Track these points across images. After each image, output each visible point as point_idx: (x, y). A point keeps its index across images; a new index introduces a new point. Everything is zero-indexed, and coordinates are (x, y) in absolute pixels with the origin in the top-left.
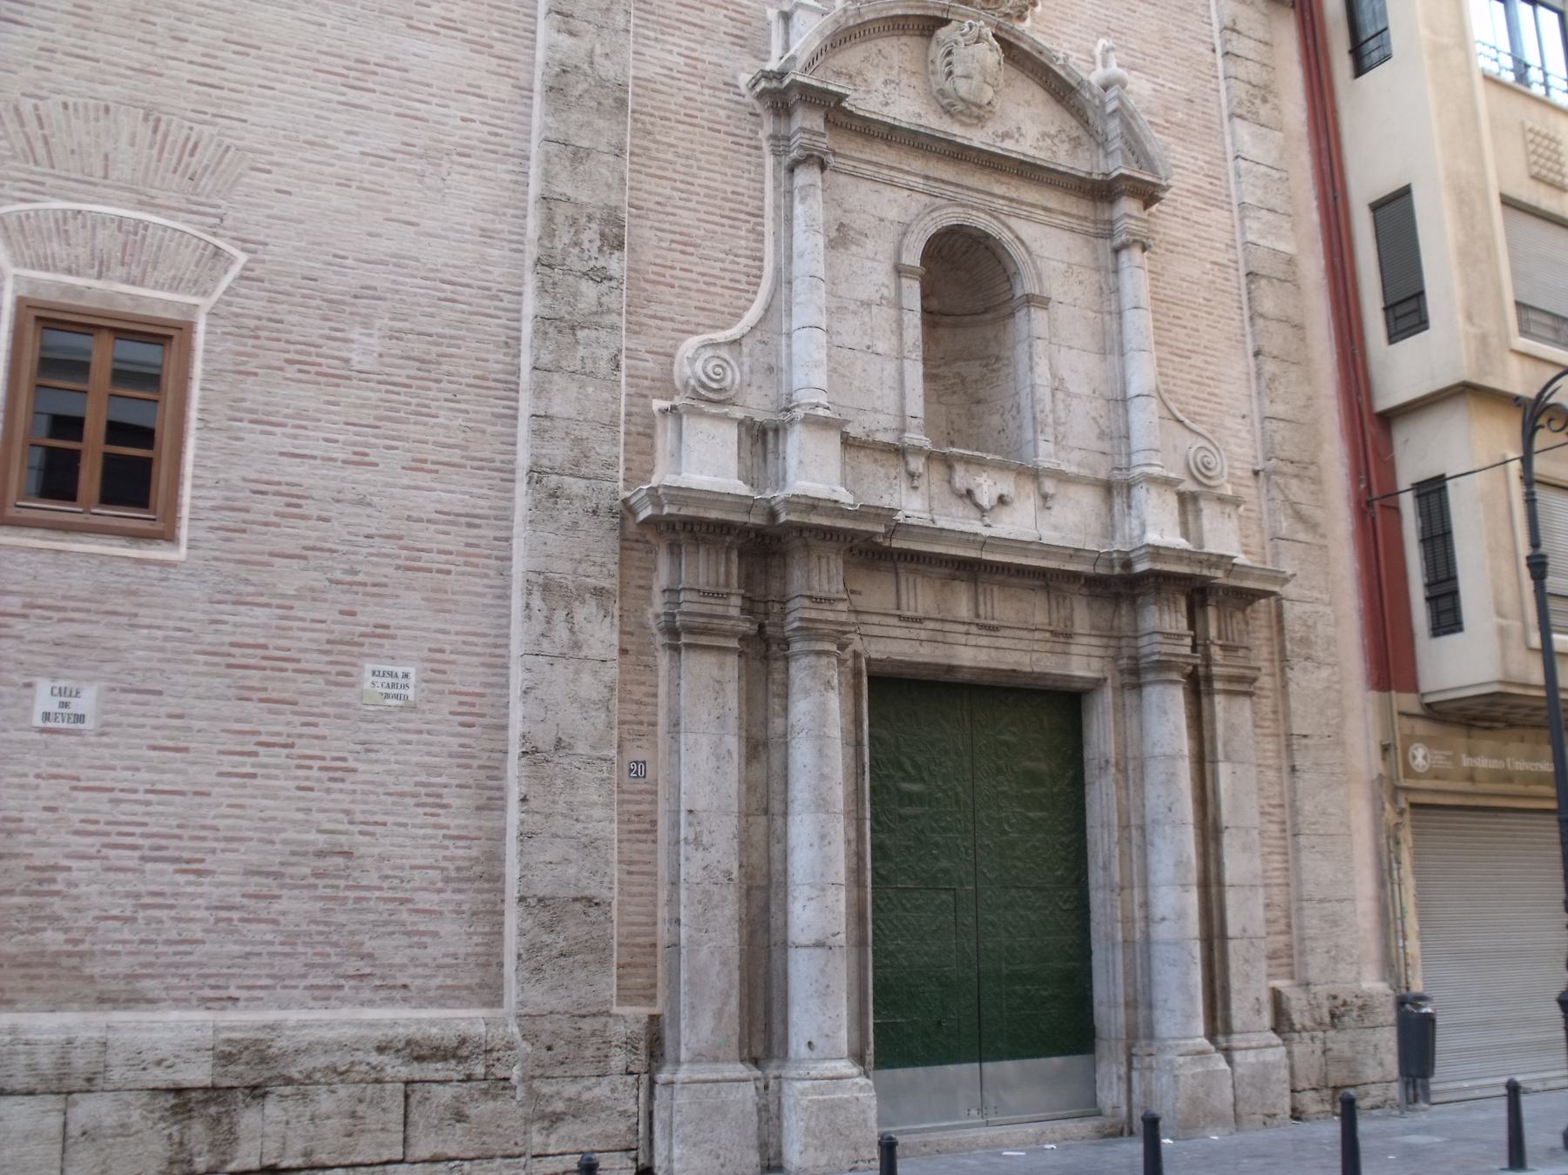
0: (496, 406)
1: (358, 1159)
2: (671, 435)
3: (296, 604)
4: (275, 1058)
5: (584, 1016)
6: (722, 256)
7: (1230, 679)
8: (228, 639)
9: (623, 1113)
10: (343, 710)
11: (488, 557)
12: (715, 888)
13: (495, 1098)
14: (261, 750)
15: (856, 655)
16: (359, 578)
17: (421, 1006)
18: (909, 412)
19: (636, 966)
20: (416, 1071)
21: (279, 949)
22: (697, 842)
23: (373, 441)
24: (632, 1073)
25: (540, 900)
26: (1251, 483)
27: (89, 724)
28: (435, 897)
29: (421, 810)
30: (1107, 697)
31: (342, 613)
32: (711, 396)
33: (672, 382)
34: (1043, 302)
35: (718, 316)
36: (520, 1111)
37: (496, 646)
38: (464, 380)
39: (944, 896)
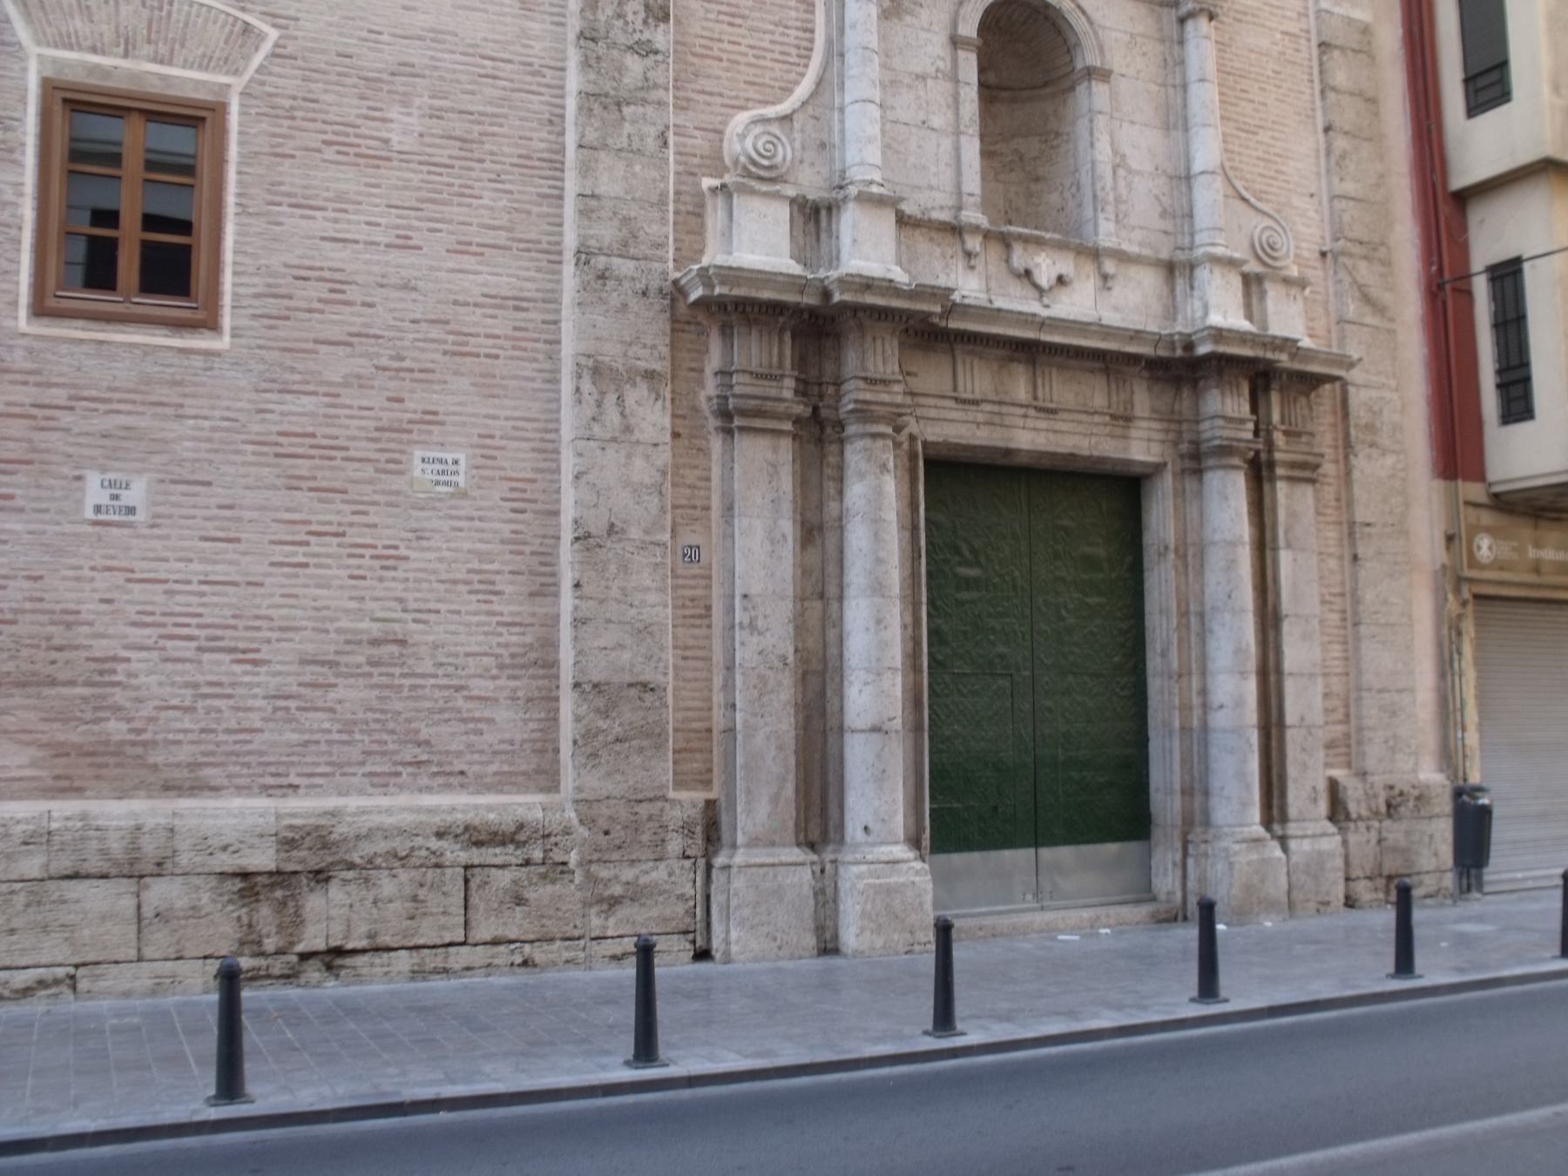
1: (421, 942)
2: (721, 214)
3: (342, 391)
4: (336, 844)
6: (771, 27)
8: (275, 428)
9: (681, 897)
10: (394, 498)
11: (536, 340)
12: (770, 673)
13: (553, 882)
14: (313, 539)
16: (407, 364)
17: (478, 792)
19: (691, 751)
20: (476, 856)
21: (336, 736)
22: (752, 626)
23: (416, 223)
24: (688, 857)
25: (595, 686)
26: (1318, 264)
27: (140, 517)
28: (491, 684)
29: (474, 597)
30: (1167, 482)
31: (390, 399)
32: (762, 173)
33: (721, 159)
34: (1105, 75)
35: (768, 90)
36: (579, 895)
37: (547, 431)
39: (1001, 682)
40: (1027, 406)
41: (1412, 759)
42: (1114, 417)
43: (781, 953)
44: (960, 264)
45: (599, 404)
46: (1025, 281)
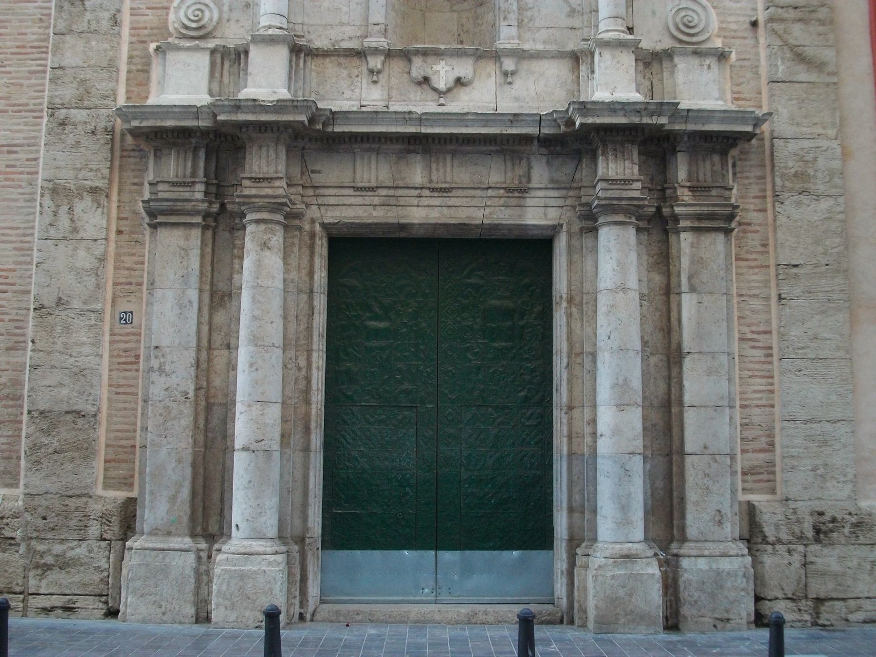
0: (32, 66)
2: (160, 68)
5: (71, 497)
7: (699, 217)
9: (97, 568)
12: (174, 405)
15: (313, 221)
18: (372, 20)
22: (161, 370)
24: (105, 540)
25: (42, 413)
26: (749, 34)
32: (192, 33)
38: (8, 51)
40: (421, 188)
41: (850, 486)
42: (508, 190)
43: (165, 618)
44: (365, 80)
45: (55, 214)
46: (425, 86)
